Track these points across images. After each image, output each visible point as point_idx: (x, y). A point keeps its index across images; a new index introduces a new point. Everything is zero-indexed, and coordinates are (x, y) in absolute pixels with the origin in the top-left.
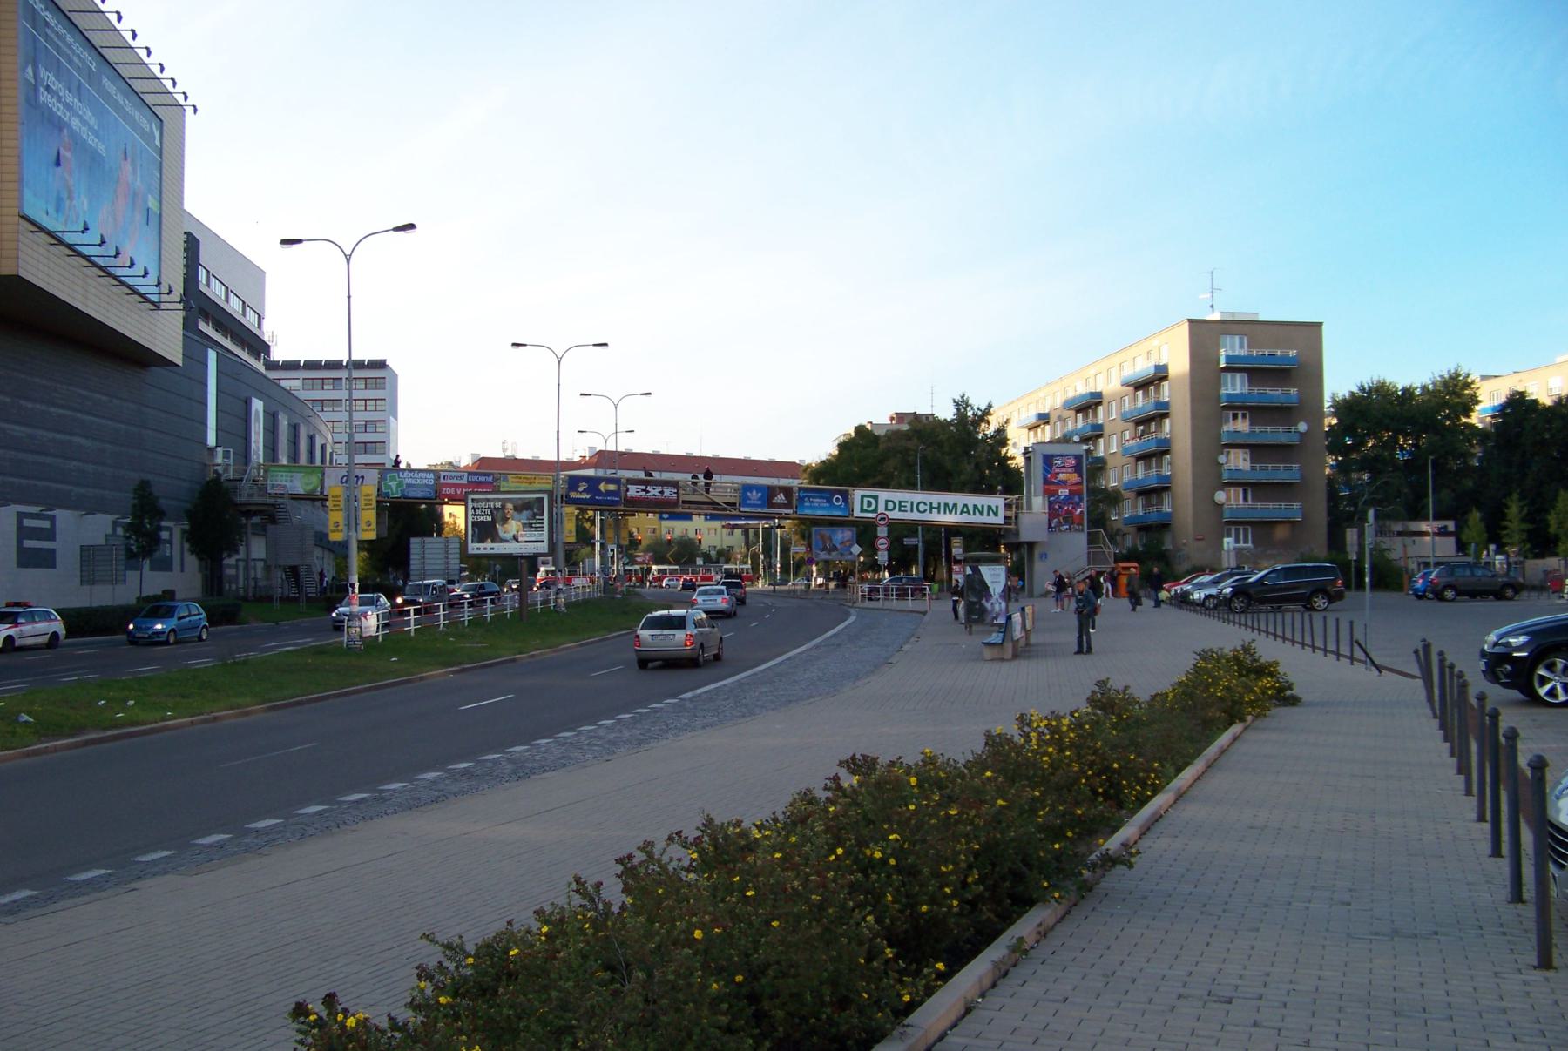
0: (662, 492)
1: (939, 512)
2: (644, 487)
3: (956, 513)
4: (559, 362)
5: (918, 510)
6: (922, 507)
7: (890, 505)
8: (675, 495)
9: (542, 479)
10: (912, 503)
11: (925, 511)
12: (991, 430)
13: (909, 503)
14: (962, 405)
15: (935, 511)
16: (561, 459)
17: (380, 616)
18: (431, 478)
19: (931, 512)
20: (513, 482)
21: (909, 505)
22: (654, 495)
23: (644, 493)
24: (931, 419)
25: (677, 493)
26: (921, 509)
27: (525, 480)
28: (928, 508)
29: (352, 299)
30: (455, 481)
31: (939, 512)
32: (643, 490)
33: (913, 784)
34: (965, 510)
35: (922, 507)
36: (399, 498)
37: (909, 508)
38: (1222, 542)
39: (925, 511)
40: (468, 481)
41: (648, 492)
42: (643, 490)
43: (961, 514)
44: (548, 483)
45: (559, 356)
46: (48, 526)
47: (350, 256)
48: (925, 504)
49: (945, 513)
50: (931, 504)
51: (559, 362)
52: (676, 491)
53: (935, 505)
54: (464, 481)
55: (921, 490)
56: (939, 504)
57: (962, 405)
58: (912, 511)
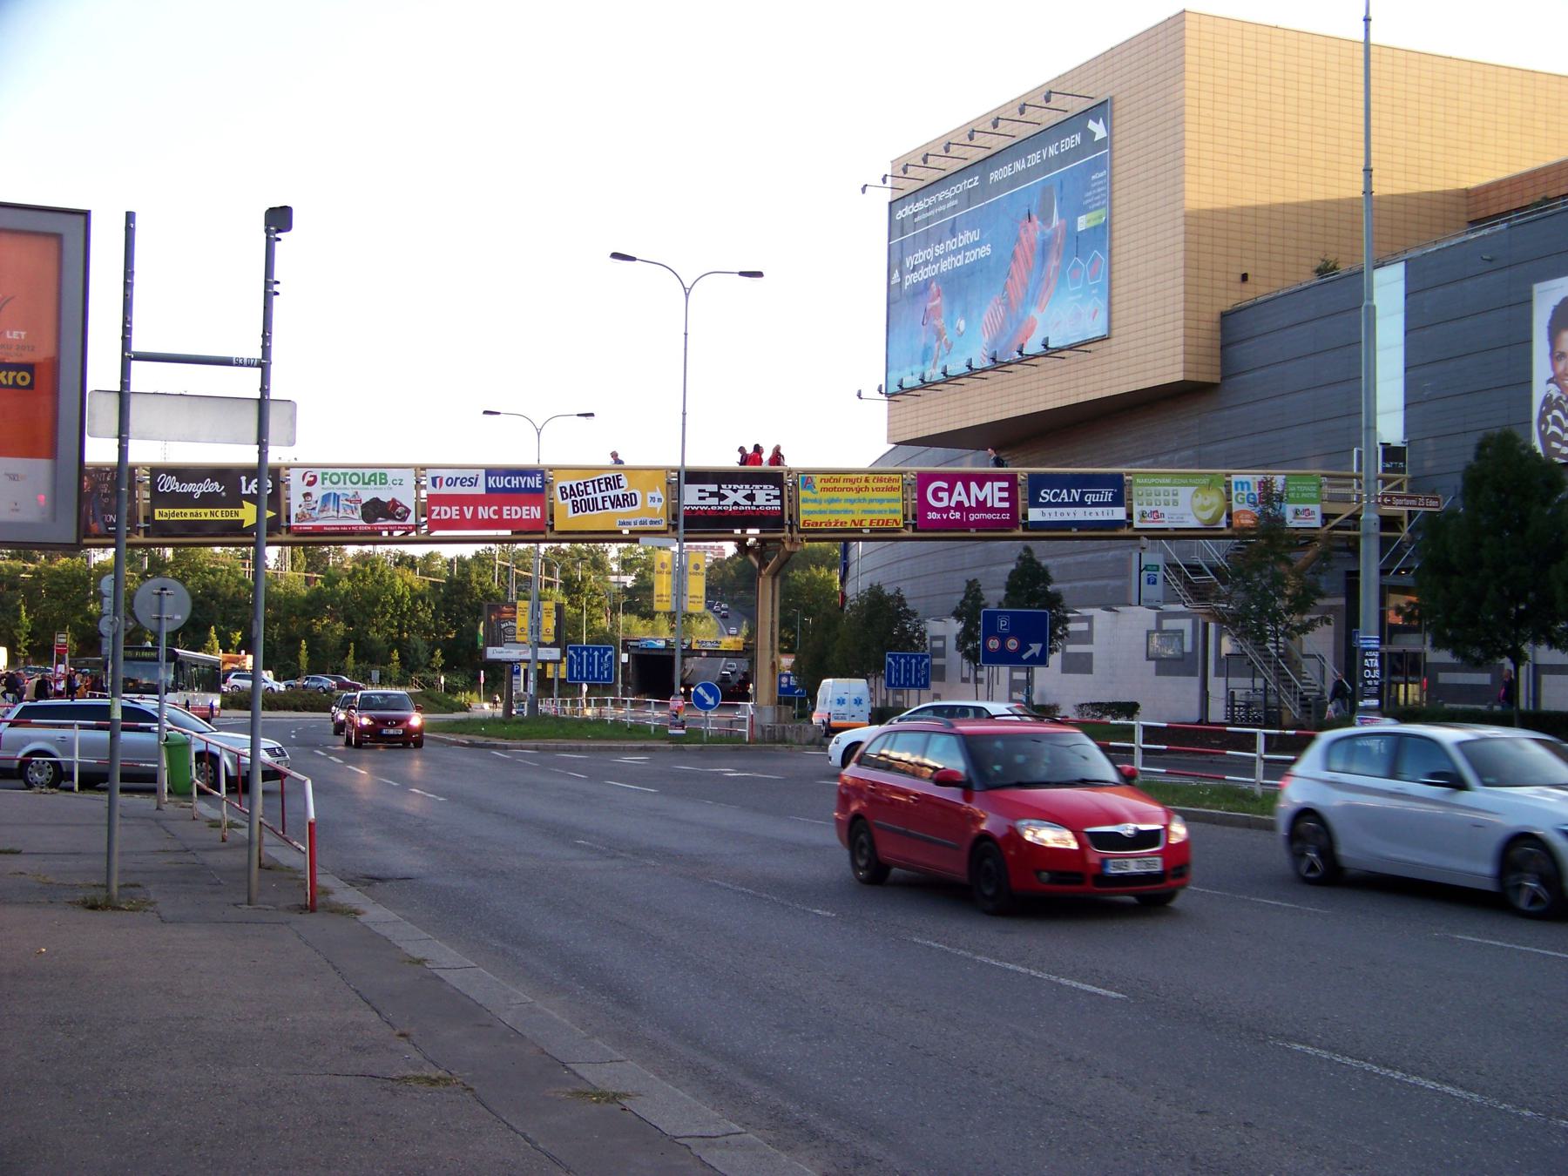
0: (751, 497)
2: (714, 488)
4: (539, 434)
5: (358, 475)
8: (778, 502)
9: (881, 480)
20: (823, 489)
22: (736, 504)
23: (715, 501)
25: (780, 497)
26: (1240, 500)
27: (848, 485)
29: (688, 336)
30: (458, 490)
32: (712, 494)
33: (499, 711)
34: (687, 291)
38: (159, 521)
40: (488, 490)
41: (723, 497)
42: (712, 494)
44: (893, 489)
45: (539, 427)
46: (1087, 629)
47: (690, 289)
51: (539, 434)
52: (777, 493)
54: (480, 490)
58: (595, 492)
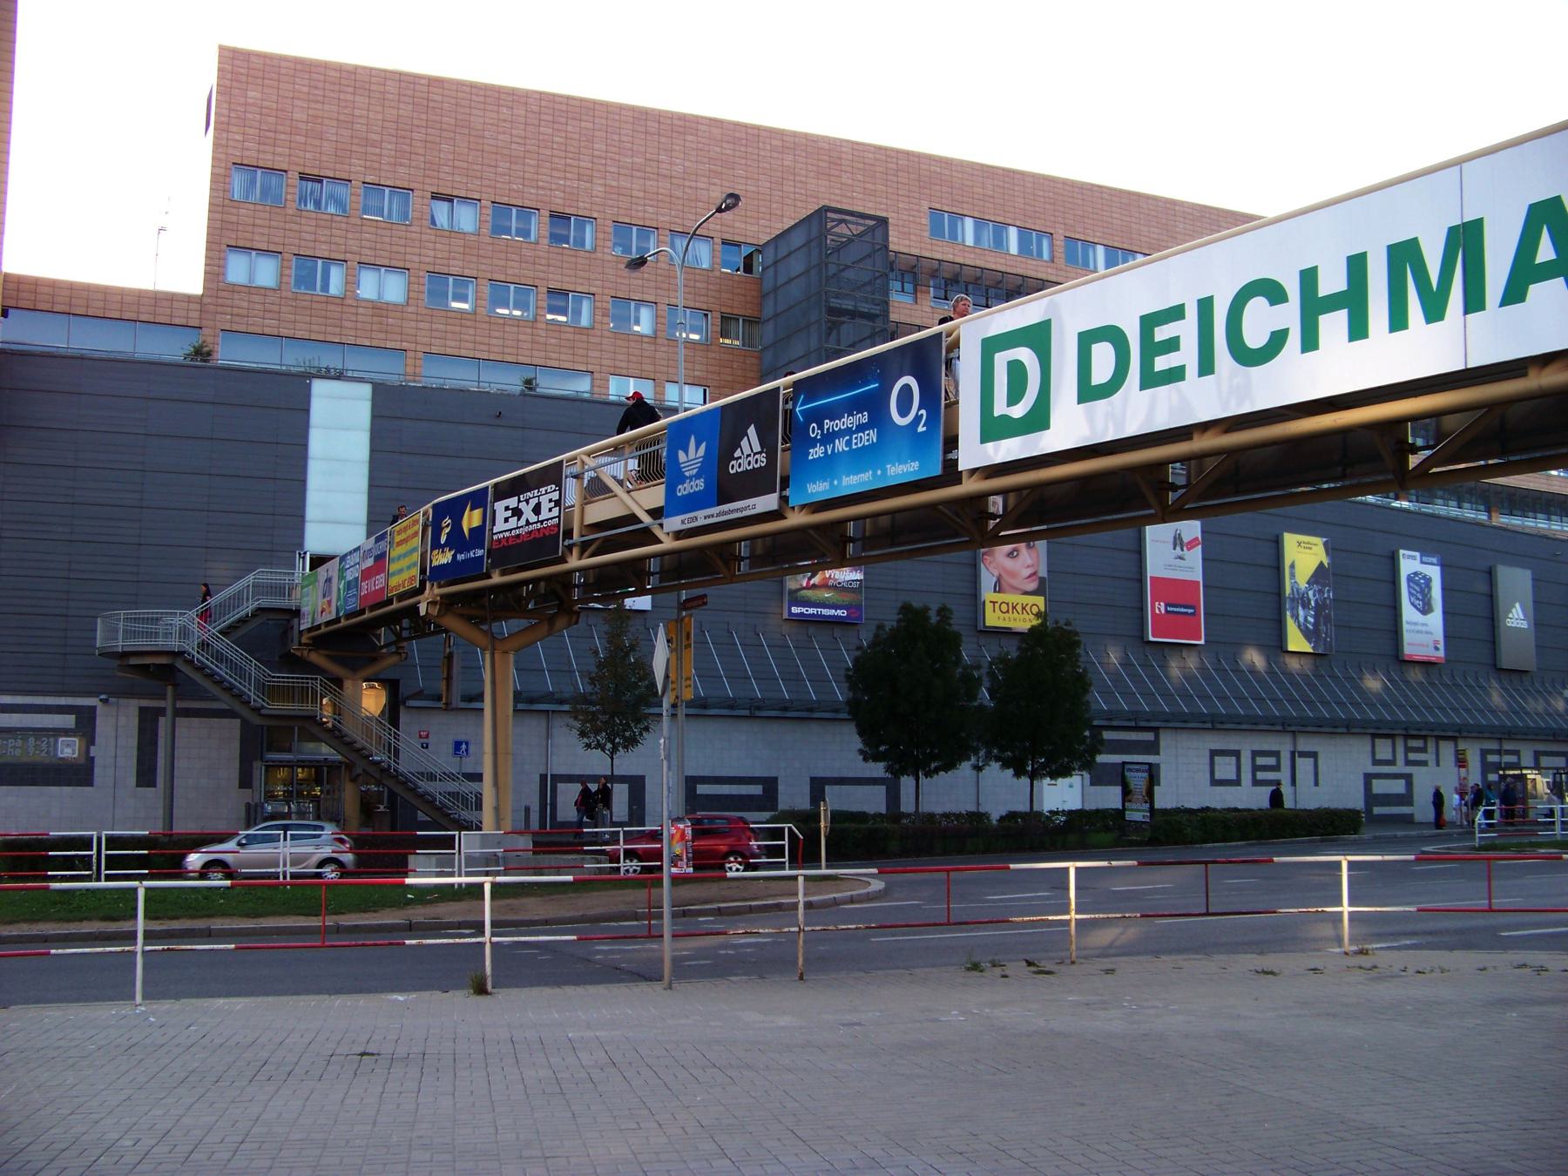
1: (1358, 330)
3: (1474, 302)
6: (1259, 322)
7: (1103, 359)
10: (1205, 306)
11: (1278, 339)
12: (901, 616)
13: (1192, 313)
14: (906, 609)
15: (1333, 325)
16: (647, 890)
17: (281, 877)
18: (1515, 512)
19: (1310, 342)
21: (1186, 331)
24: (581, 805)
28: (1289, 315)
31: (1358, 330)
35: (1259, 322)
36: (337, 620)
37: (1187, 355)
39: (1278, 339)
43: (1514, 294)
48: (1273, 292)
49: (1398, 321)
50: (1309, 278)
53: (1332, 282)
55: (803, 862)
56: (1357, 265)
57: (906, 609)
58: (1206, 366)
